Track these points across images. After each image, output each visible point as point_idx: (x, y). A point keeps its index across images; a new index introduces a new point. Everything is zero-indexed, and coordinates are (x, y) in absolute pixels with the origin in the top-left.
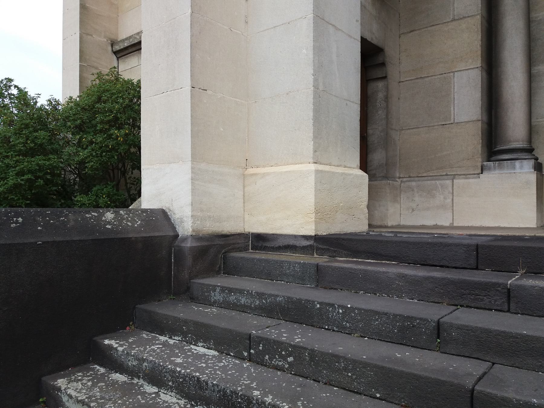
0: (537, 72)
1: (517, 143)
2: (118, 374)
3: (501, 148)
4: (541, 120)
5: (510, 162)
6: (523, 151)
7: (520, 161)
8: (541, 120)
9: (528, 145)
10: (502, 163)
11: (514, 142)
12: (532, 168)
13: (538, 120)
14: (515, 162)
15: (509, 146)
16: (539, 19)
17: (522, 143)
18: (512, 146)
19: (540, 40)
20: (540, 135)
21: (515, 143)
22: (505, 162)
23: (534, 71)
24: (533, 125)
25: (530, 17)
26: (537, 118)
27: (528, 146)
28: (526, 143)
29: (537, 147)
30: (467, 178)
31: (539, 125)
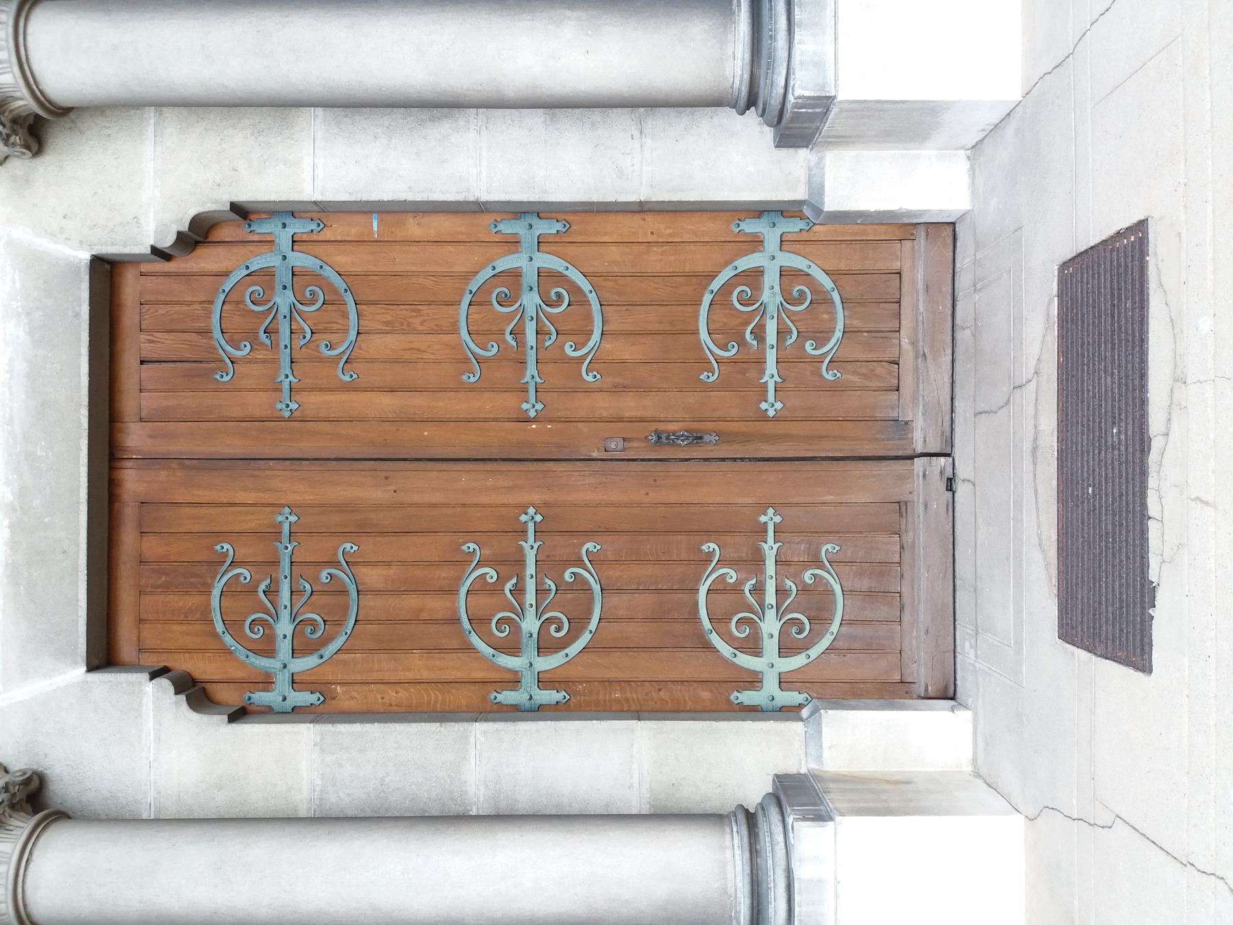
0: (486, 786)
1: (729, 867)
2: (505, 692)
3: (742, 918)
4: (636, 776)
5: (800, 893)
6: (756, 848)
7: (797, 863)
8: (636, 776)
9: (735, 829)
10: (800, 920)
11: (725, 879)
12: (822, 827)
13: (636, 784)
14: (799, 879)
15: (740, 895)
16: (319, 782)
17: (729, 853)
18: (740, 885)
19: (387, 780)
20: (683, 779)
21: (730, 876)
22: (799, 912)
23: (482, 796)
24: (650, 798)
25: (164, 109)
26: (629, 788)
27: (737, 832)
28: (728, 837)
29: (719, 786)
30: (332, 395)
31: (651, 781)
